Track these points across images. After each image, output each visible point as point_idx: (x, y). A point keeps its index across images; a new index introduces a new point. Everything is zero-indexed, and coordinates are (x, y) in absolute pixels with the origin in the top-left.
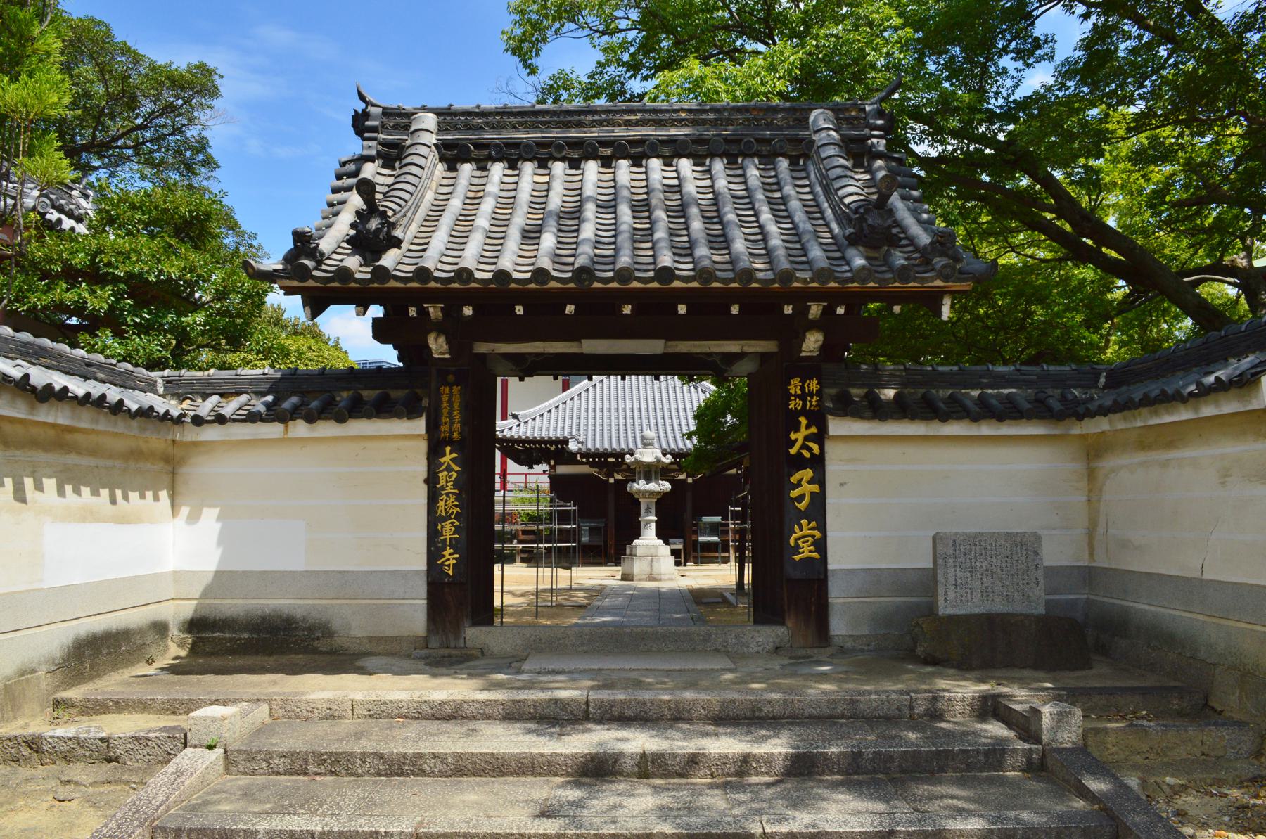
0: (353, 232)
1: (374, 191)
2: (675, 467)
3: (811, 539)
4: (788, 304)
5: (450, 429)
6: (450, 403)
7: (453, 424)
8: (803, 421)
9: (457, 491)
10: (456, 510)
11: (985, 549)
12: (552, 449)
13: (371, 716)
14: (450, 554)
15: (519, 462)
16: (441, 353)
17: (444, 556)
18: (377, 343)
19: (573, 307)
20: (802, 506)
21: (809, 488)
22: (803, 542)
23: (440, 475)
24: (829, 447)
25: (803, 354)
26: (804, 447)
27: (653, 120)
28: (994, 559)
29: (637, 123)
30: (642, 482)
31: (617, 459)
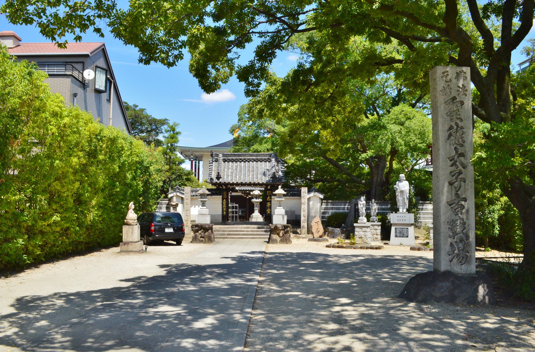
7: (225, 196)
30: (255, 199)
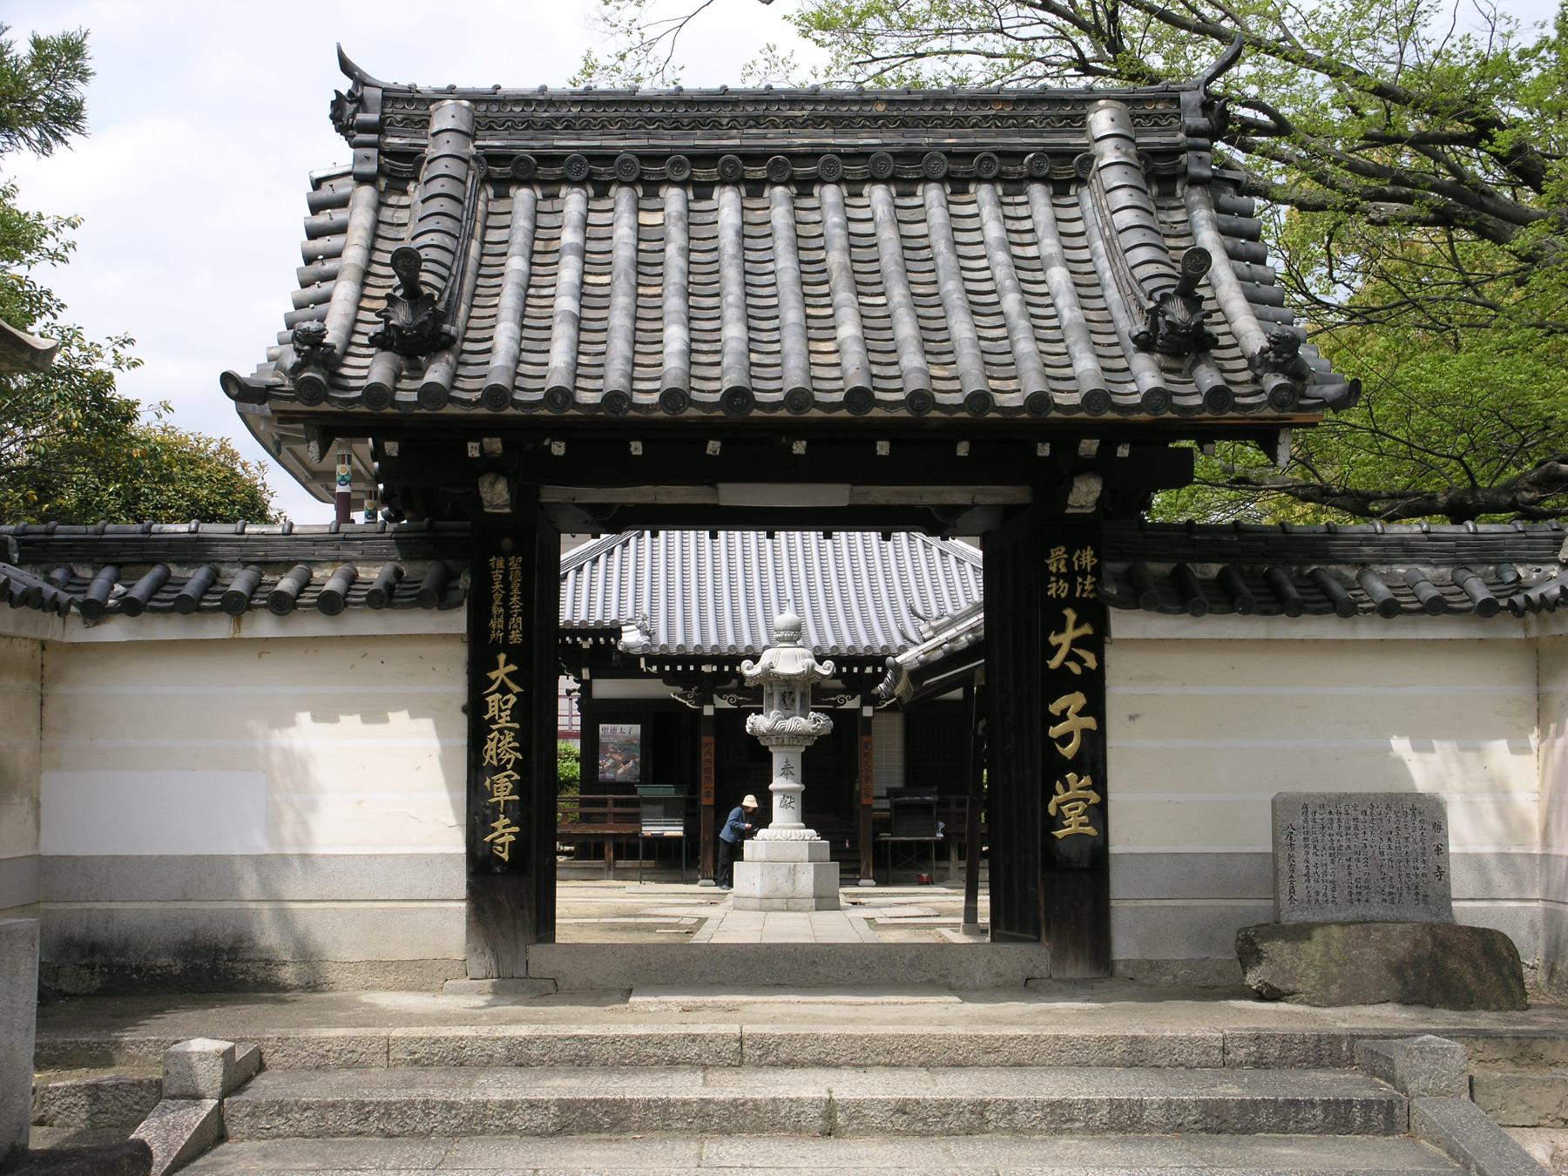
1: (418, 268)
2: (838, 683)
3: (1082, 806)
4: (1044, 442)
5: (506, 624)
6: (506, 583)
8: (1070, 615)
9: (517, 726)
10: (515, 755)
11: (1355, 819)
12: (586, 646)
13: (416, 1062)
14: (505, 827)
17: (494, 830)
19: (718, 444)
20: (1069, 751)
21: (1075, 724)
22: (1070, 810)
23: (489, 699)
25: (1069, 511)
26: (1071, 656)
27: (832, 118)
28: (1368, 836)
29: (804, 124)
31: (720, 668)
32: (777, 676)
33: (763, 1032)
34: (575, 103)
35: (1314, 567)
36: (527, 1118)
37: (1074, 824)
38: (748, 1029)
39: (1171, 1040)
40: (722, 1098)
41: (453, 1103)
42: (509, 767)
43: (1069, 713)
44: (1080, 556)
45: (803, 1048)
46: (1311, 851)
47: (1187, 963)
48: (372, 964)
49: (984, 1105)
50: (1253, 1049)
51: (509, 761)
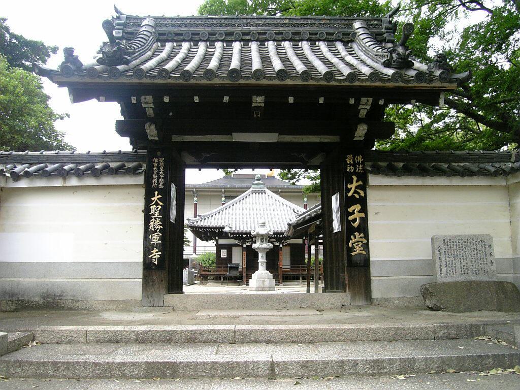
0: (101, 55)
4: (352, 98)
5: (158, 181)
6: (158, 167)
8: (355, 178)
9: (161, 217)
12: (217, 232)
15: (202, 239)
16: (153, 136)
17: (152, 253)
18: (117, 135)
19: (228, 98)
20: (356, 225)
21: (357, 215)
22: (357, 245)
23: (151, 207)
24: (368, 190)
26: (355, 192)
28: (467, 250)
32: (260, 234)
33: (244, 328)
34: (189, 19)
35: (434, 164)
36: (131, 370)
37: (358, 250)
38: (238, 327)
39: (413, 328)
40: (222, 361)
41: (98, 363)
42: (158, 231)
43: (355, 212)
44: (357, 158)
45: (261, 335)
46: (447, 256)
47: (398, 299)
48: (109, 301)
49: (343, 362)
50: (446, 331)
51: (158, 229)
